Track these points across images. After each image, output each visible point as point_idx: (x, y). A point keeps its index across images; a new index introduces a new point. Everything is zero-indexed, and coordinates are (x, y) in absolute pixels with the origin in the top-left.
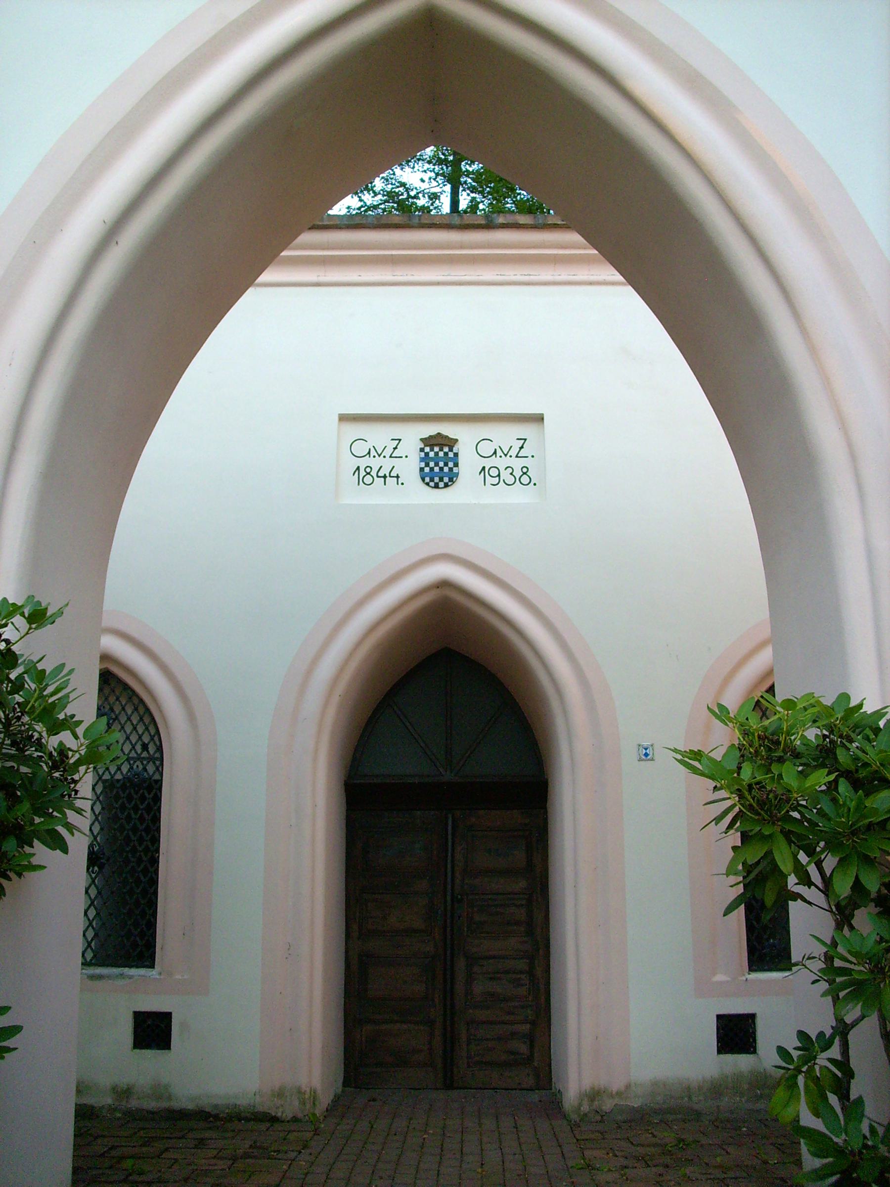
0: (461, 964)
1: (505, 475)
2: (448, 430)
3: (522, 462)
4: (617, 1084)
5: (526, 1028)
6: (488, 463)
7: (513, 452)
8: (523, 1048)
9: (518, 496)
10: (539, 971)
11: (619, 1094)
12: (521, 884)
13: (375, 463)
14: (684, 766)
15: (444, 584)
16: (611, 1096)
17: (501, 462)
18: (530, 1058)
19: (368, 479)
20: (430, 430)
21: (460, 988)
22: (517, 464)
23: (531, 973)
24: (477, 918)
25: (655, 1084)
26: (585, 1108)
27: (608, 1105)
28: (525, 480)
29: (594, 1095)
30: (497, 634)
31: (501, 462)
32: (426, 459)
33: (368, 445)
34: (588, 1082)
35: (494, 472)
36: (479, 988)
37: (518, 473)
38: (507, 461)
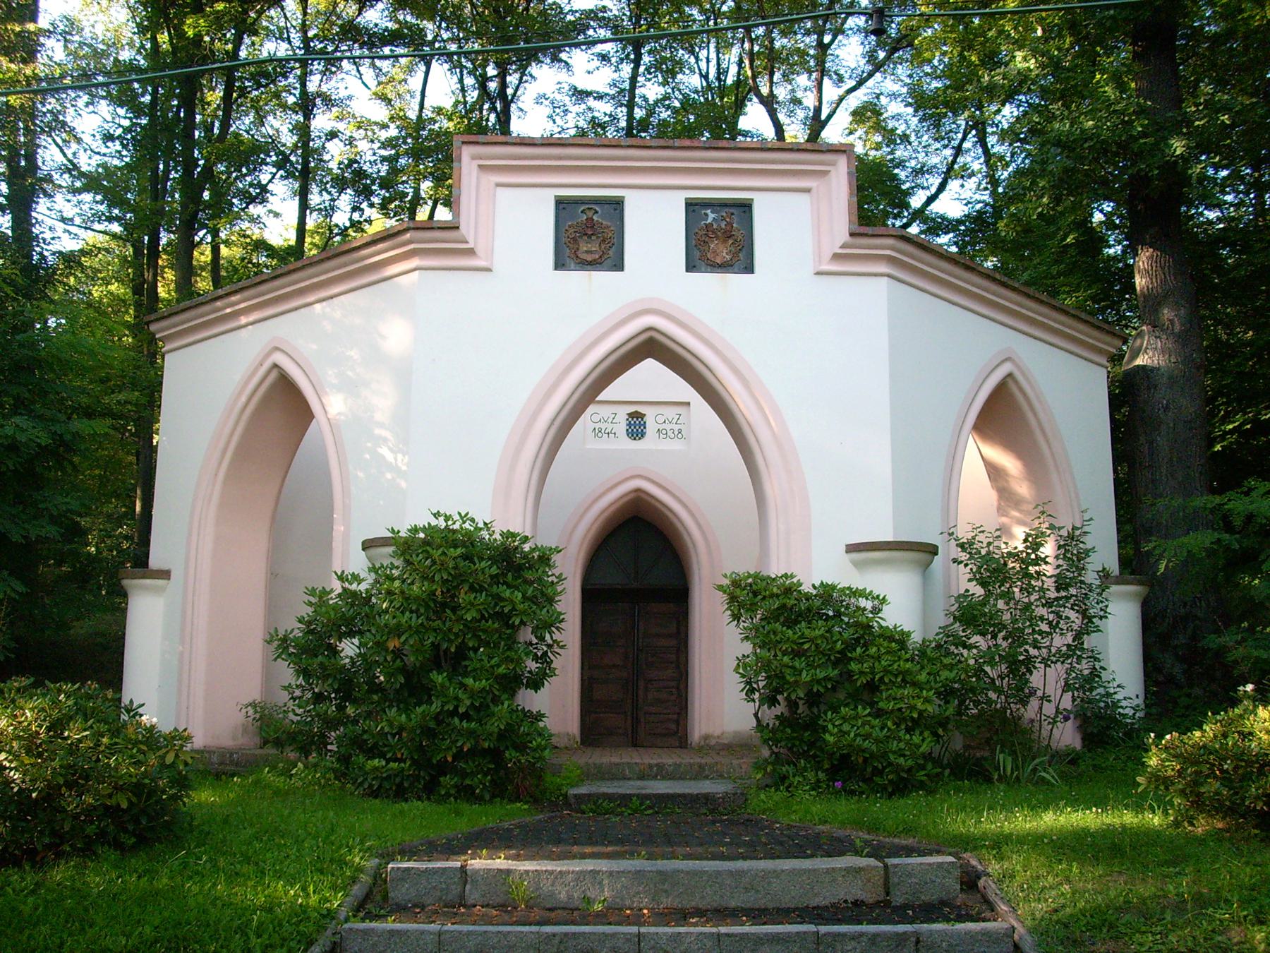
0: (641, 684)
1: (670, 433)
2: (641, 409)
3: (679, 427)
4: (717, 732)
5: (675, 716)
6: (661, 427)
7: (674, 421)
8: (673, 726)
9: (676, 445)
10: (682, 686)
11: (718, 737)
12: (674, 642)
13: (603, 426)
14: (298, 224)
15: (638, 490)
16: (714, 738)
17: (668, 427)
18: (677, 732)
19: (600, 435)
20: (632, 409)
21: (641, 693)
22: (676, 428)
23: (678, 688)
24: (650, 659)
25: (735, 732)
26: (702, 743)
27: (713, 742)
28: (680, 436)
29: (706, 737)
30: (650, 504)
31: (668, 427)
32: (629, 425)
33: (600, 416)
34: (703, 732)
35: (664, 432)
36: (650, 696)
37: (676, 433)
38: (671, 426)
